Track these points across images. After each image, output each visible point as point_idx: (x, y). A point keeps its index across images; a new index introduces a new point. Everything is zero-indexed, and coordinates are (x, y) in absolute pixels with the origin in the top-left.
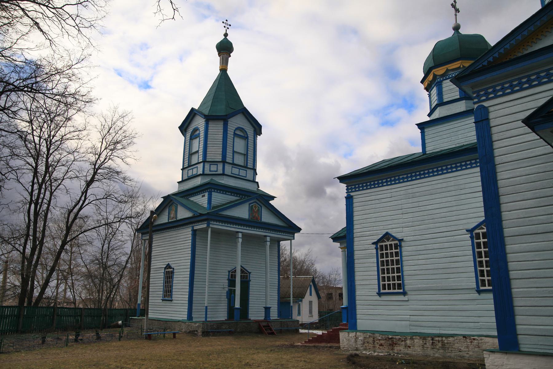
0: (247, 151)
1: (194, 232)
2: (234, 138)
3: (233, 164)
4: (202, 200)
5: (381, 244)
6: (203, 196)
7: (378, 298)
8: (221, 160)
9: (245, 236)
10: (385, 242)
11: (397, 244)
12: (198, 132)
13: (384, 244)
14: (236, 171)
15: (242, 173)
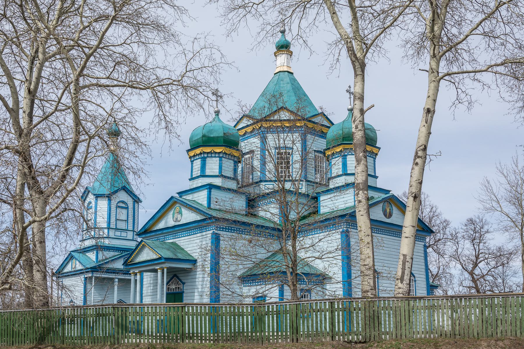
0: (128, 217)
1: (86, 278)
2: (116, 209)
3: (116, 229)
4: (92, 256)
6: (93, 253)
8: (106, 227)
9: (120, 280)
12: (91, 205)
14: (118, 233)
15: (124, 234)
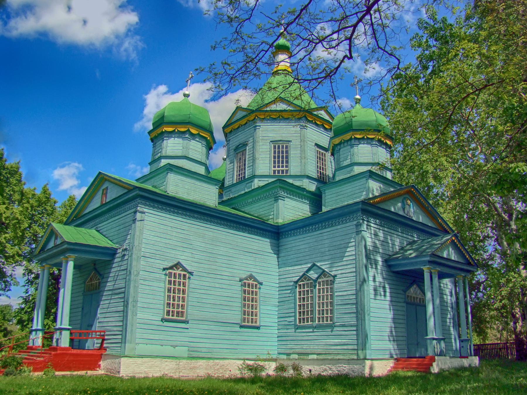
5: (171, 271)
7: (161, 323)
10: (174, 270)
11: (312, 283)
13: (173, 272)
